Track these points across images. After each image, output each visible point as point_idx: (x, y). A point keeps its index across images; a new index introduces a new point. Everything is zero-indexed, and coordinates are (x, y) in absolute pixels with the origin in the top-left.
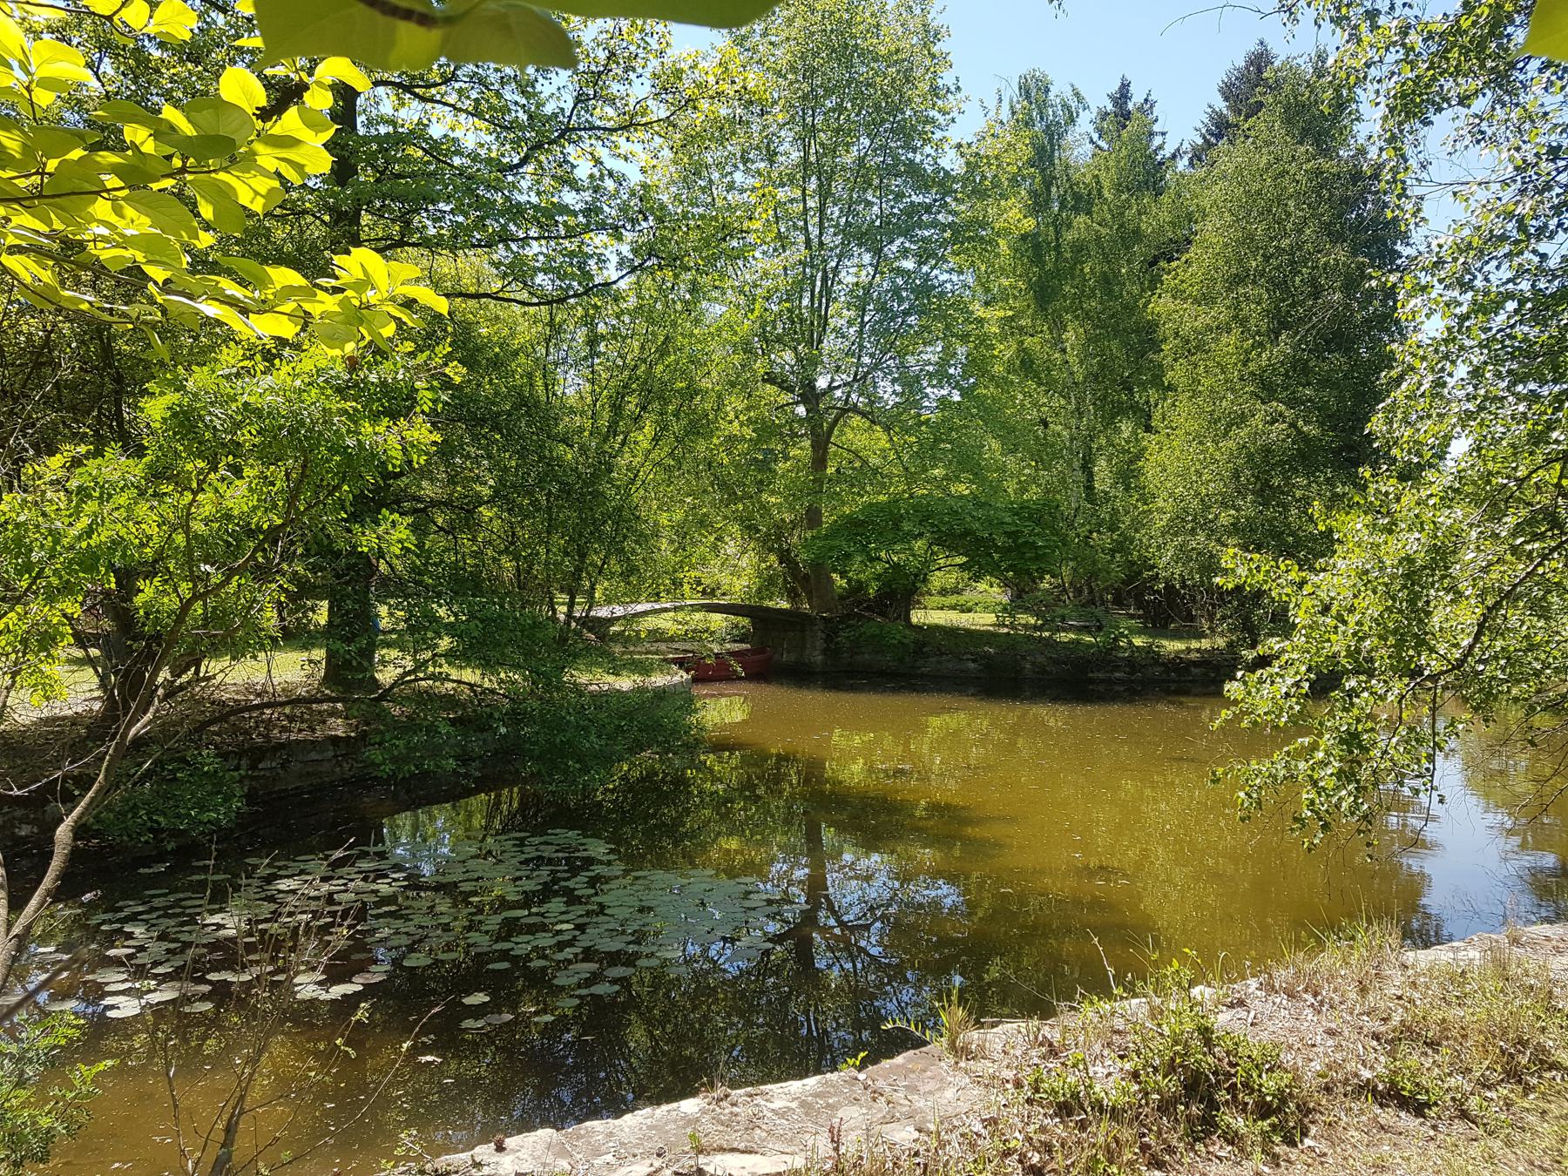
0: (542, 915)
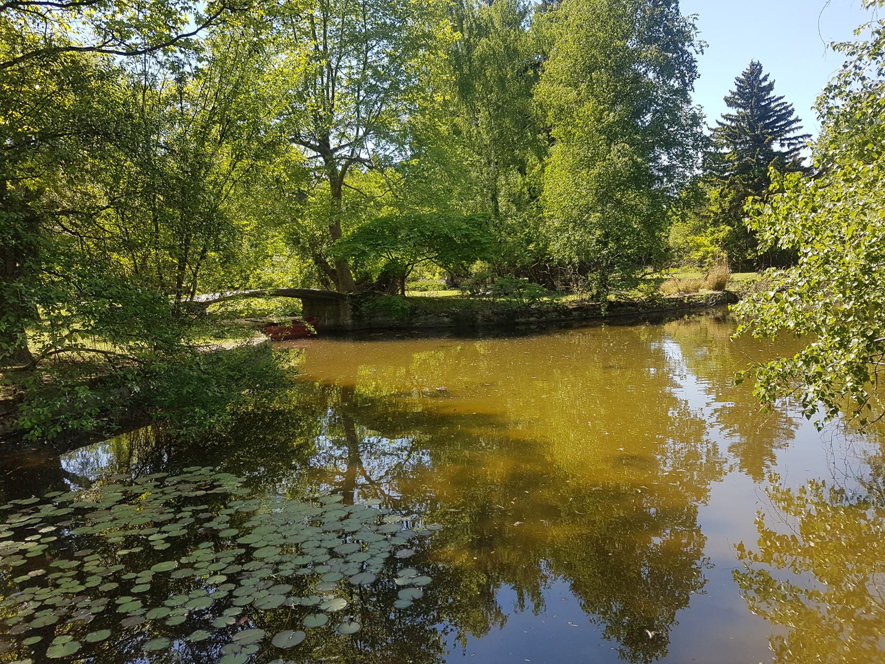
0: (191, 565)
